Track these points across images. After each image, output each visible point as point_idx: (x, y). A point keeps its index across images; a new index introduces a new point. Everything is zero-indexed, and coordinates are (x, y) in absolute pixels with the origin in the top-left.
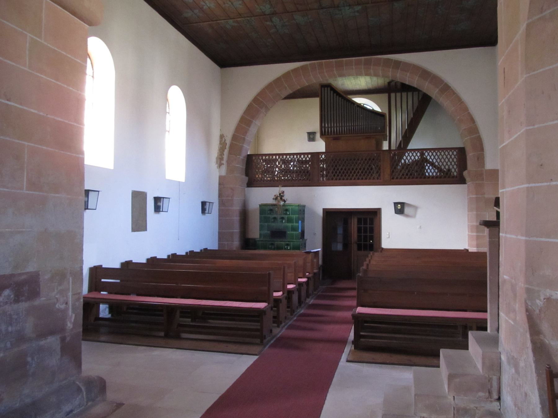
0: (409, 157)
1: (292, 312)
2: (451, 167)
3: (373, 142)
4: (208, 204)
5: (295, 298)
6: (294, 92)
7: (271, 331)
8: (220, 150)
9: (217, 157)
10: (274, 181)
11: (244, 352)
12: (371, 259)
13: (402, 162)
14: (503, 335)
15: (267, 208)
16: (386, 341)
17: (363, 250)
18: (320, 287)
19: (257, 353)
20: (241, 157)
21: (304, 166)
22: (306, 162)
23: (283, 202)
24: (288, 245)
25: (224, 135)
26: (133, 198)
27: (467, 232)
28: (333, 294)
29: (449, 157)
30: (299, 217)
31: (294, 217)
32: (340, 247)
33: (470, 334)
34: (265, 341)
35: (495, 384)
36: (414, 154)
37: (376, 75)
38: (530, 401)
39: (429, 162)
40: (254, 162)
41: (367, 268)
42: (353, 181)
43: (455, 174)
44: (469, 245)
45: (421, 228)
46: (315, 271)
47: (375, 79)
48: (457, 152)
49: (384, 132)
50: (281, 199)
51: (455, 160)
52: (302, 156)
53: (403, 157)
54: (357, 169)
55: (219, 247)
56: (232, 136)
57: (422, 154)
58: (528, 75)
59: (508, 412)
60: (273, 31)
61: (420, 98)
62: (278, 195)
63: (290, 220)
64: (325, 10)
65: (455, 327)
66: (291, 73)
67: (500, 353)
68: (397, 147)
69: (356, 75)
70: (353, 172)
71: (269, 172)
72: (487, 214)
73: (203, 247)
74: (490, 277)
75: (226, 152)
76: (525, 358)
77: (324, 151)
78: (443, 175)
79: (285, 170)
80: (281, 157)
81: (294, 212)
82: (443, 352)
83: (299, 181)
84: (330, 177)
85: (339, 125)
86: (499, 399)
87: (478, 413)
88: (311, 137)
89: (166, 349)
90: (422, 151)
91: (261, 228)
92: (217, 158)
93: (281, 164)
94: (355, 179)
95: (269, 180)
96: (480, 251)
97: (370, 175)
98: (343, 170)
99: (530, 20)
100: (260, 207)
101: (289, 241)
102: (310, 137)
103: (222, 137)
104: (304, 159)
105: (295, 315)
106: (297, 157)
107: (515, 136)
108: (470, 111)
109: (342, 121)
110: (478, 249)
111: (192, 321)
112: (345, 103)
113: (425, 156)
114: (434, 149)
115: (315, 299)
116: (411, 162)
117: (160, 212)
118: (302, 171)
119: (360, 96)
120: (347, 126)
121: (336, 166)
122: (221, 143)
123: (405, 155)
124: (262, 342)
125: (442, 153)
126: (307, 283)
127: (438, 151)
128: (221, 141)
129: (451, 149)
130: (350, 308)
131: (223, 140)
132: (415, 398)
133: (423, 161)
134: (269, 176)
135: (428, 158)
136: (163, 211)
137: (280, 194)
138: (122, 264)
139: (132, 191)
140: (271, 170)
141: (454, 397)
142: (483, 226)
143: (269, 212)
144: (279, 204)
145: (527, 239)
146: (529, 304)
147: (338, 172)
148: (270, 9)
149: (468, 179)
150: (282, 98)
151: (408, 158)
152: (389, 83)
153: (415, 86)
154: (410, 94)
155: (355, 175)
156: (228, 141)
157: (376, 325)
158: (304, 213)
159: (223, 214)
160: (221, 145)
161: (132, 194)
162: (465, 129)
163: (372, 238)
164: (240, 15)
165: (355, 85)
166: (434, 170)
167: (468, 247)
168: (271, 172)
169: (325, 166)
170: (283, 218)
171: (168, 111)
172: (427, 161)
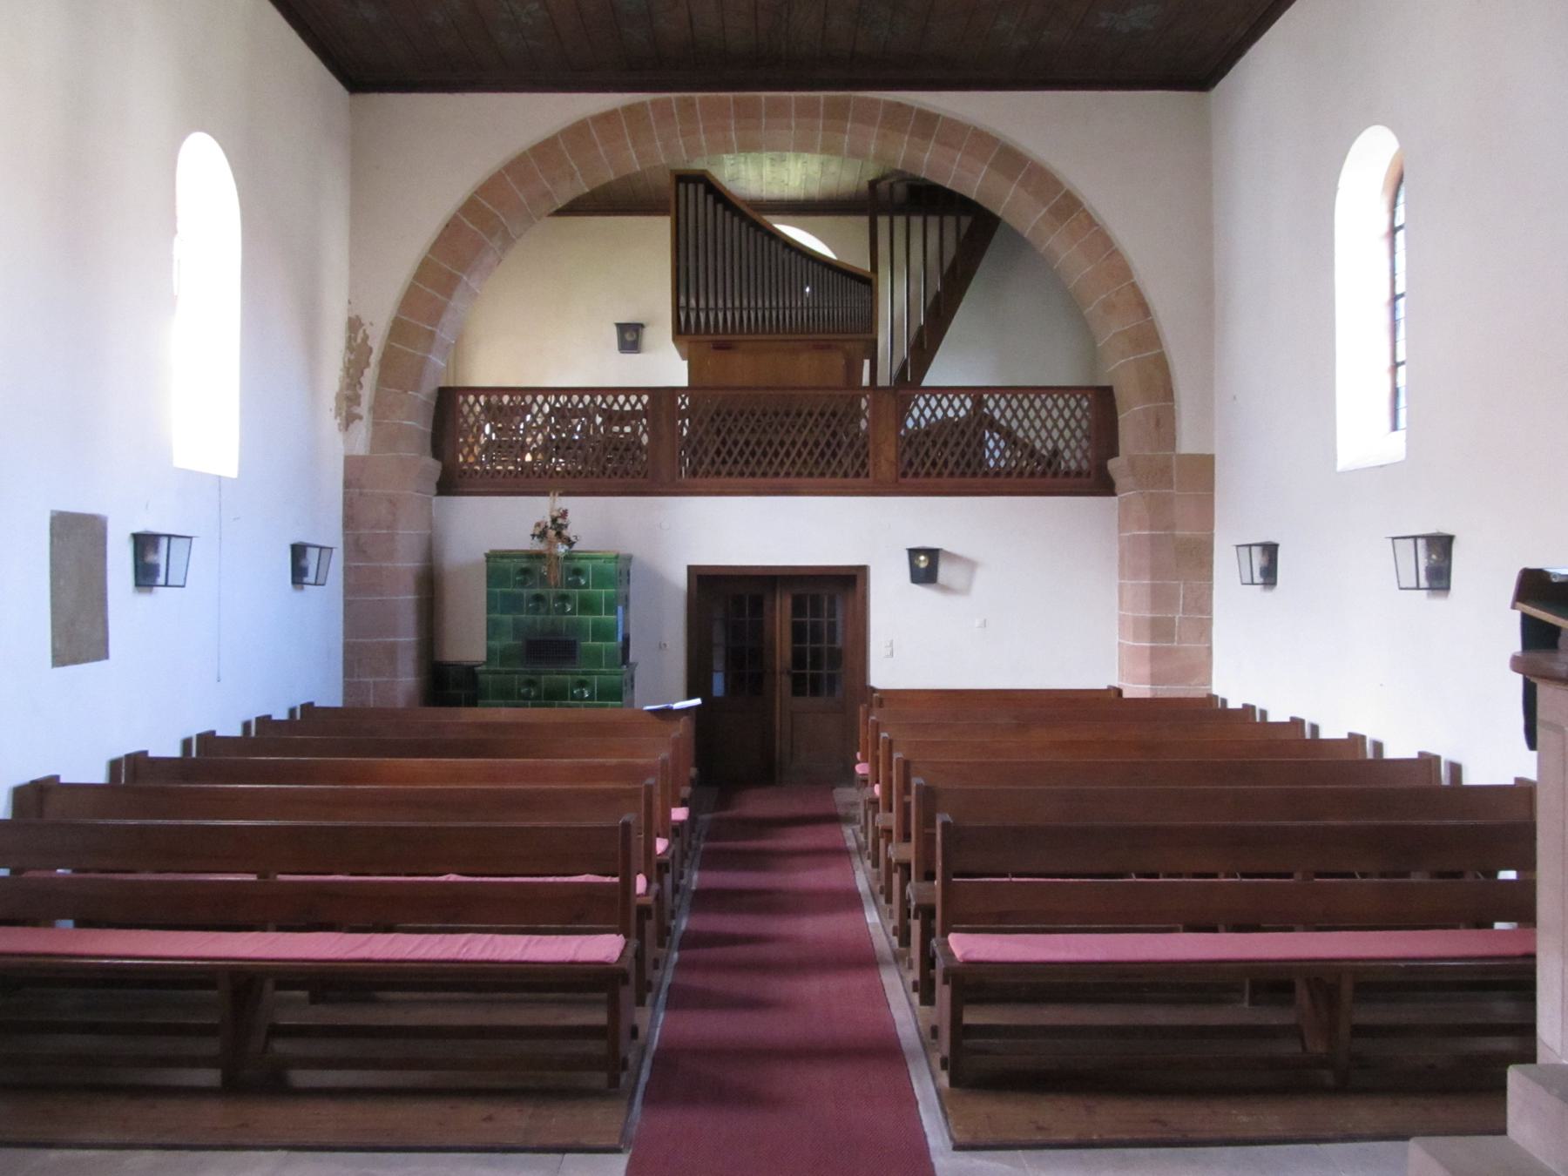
0: (1020, 410)
2: (1061, 444)
3: (839, 361)
8: (347, 370)
11: (568, 1141)
17: (808, 692)
19: (615, 1141)
20: (421, 396)
21: (579, 428)
22: (623, 417)
23: (566, 547)
24: (582, 684)
25: (363, 321)
26: (55, 540)
27: (1117, 637)
42: (780, 480)
50: (559, 534)
51: (1084, 424)
54: (793, 443)
55: (345, 701)
57: (979, 403)
62: (549, 524)
63: (587, 606)
70: (782, 452)
72: (1182, 586)
73: (298, 700)
75: (370, 376)
83: (586, 477)
88: (630, 337)
89: (245, 1154)
91: (493, 629)
94: (788, 474)
100: (487, 561)
101: (585, 673)
102: (626, 341)
103: (354, 325)
104: (627, 408)
108: (1135, 278)
110: (1154, 687)
112: (751, 235)
113: (986, 410)
117: (155, 589)
118: (623, 447)
119: (814, 254)
120: (733, 308)
124: (614, 1081)
128: (350, 340)
129: (957, 390)
131: (360, 335)
135: (997, 414)
136: (170, 583)
137: (554, 520)
139: (52, 511)
143: (518, 578)
144: (553, 551)
149: (1120, 481)
151: (922, 413)
153: (973, 196)
155: (788, 462)
159: (357, 587)
160: (351, 353)
165: (770, 183)
167: (1119, 681)
170: (564, 598)
172: (993, 425)
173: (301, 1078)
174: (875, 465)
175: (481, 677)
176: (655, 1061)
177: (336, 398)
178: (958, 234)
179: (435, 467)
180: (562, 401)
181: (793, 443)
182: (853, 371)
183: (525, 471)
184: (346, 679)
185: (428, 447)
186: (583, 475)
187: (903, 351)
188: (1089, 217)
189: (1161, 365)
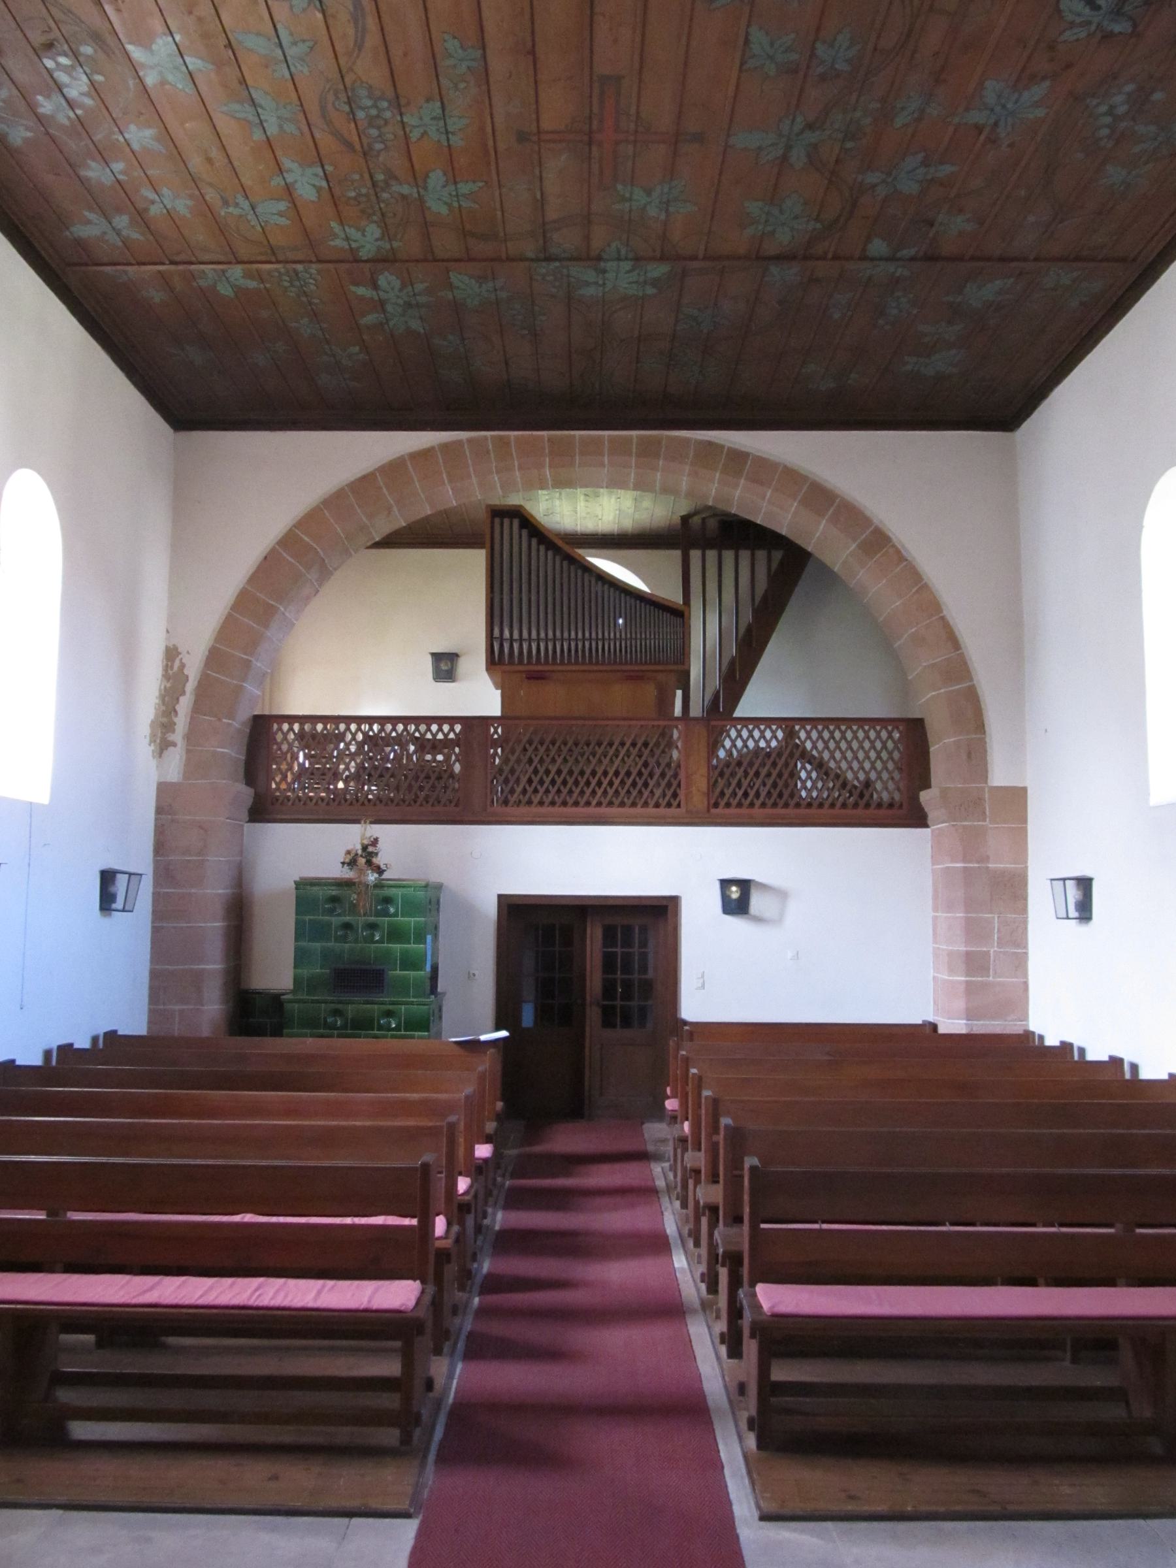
2: (873, 775)
4: (121, 880)
8: (162, 697)
9: (153, 722)
13: (718, 756)
15: (320, 893)
19: (404, 1505)
20: (237, 725)
22: (444, 745)
23: (376, 875)
24: (389, 1014)
27: (932, 971)
30: (425, 921)
31: (411, 922)
42: (591, 810)
44: (936, 1012)
45: (798, 958)
48: (900, 733)
49: (683, 664)
50: (369, 863)
51: (896, 755)
52: (434, 728)
54: (605, 773)
57: (791, 734)
60: (370, 319)
62: (360, 852)
63: (396, 934)
64: (557, 264)
66: (466, 446)
70: (594, 782)
75: (185, 704)
85: (538, 634)
90: (788, 724)
91: (301, 957)
92: (153, 724)
94: (599, 804)
98: (551, 776)
100: (296, 889)
101: (393, 1003)
103: (171, 654)
104: (440, 736)
110: (969, 1022)
113: (797, 741)
122: (166, 676)
124: (406, 1439)
127: (801, 726)
128: (166, 668)
131: (177, 664)
135: (808, 745)
137: (365, 848)
148: (379, 243)
149: (932, 815)
150: (369, 544)
156: (193, 667)
162: (933, 665)
164: (274, 253)
165: (585, 518)
167: (934, 1015)
175: (287, 1006)
179: (246, 793)
182: (665, 703)
187: (715, 682)
188: (898, 552)
189: (972, 698)
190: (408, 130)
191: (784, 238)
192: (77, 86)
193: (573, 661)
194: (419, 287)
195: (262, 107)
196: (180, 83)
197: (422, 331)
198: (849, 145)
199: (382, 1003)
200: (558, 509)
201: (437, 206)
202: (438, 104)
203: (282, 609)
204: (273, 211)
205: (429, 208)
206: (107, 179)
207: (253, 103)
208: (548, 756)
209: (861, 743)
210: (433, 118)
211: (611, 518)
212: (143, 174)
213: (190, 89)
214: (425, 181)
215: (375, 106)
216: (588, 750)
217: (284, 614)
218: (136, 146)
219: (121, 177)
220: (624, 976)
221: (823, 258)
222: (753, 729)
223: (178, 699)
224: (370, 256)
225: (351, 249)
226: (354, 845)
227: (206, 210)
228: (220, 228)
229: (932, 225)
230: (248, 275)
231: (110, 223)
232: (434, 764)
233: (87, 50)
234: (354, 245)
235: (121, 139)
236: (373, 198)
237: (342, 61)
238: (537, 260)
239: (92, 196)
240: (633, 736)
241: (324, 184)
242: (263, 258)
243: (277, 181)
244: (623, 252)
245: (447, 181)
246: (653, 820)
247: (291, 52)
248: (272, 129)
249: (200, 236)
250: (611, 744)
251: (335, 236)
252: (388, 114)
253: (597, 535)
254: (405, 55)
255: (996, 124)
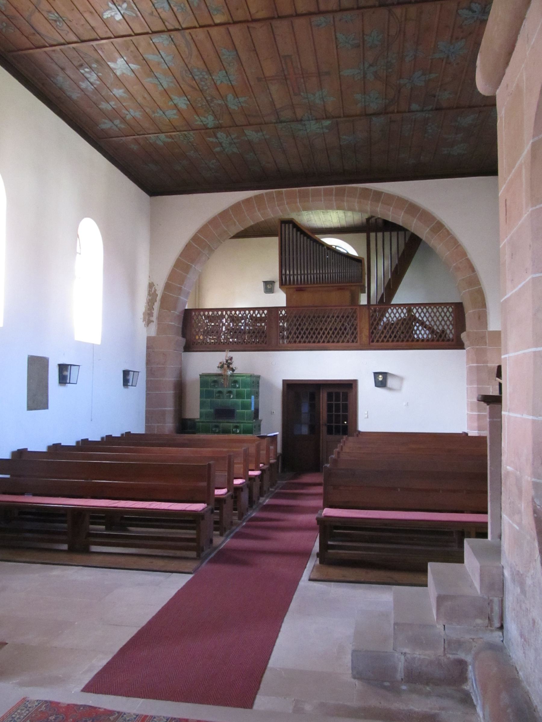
1: (241, 516)
2: (446, 327)
3: (347, 294)
4: (131, 373)
5: (244, 496)
6: (245, 229)
7: (211, 541)
10: (219, 344)
12: (344, 445)
13: (383, 321)
14: (506, 544)
15: (210, 379)
16: (360, 552)
18: (279, 482)
19: (191, 570)
20: (177, 313)
22: (261, 320)
23: (231, 372)
24: (237, 427)
27: (466, 411)
28: (291, 491)
29: (443, 314)
32: (305, 430)
33: (466, 542)
34: (203, 554)
35: (496, 608)
36: (400, 311)
37: (351, 209)
38: (539, 631)
39: (418, 321)
40: (193, 318)
41: (339, 457)
42: (321, 344)
43: (451, 336)
44: (469, 427)
46: (272, 461)
47: (349, 214)
48: (452, 308)
50: (228, 367)
51: (451, 318)
53: (386, 314)
54: (326, 329)
55: (146, 430)
56: (165, 285)
57: (409, 311)
58: (534, 208)
59: (512, 644)
60: (218, 149)
61: (407, 239)
62: (225, 363)
63: (239, 395)
64: (285, 124)
65: (450, 533)
67: (503, 567)
68: (378, 301)
69: (326, 209)
70: (321, 333)
71: (213, 332)
74: (490, 469)
75: (157, 305)
76: (532, 574)
77: (284, 305)
78: (436, 338)
79: (233, 329)
80: (229, 312)
81: (245, 385)
82: (431, 566)
83: (251, 344)
84: (292, 339)
86: (501, 628)
87: (475, 646)
88: (269, 287)
90: (409, 307)
91: (202, 405)
92: (144, 314)
93: (229, 322)
94: (324, 342)
95: (212, 342)
96: (482, 435)
97: (343, 337)
99: (536, 139)
100: (200, 377)
104: (259, 316)
105: (244, 520)
106: (249, 313)
107: (520, 286)
109: (322, 269)
111: (107, 529)
113: (413, 314)
114: (425, 305)
115: (271, 498)
116: (396, 321)
117: (67, 384)
118: (256, 332)
121: (300, 325)
122: (149, 294)
123: (388, 312)
125: (435, 310)
126: (261, 477)
128: (149, 291)
129: (445, 304)
130: (315, 510)
131: (153, 290)
132: (394, 628)
133: (410, 319)
134: (213, 338)
135: (417, 315)
137: (227, 361)
138: (14, 454)
139: (28, 356)
140: (215, 330)
141: (444, 626)
142: (483, 402)
145: (535, 418)
146: (537, 503)
147: (321, 333)
148: (214, 122)
149: (466, 343)
150: (230, 237)
152: (368, 220)
153: (401, 224)
154: (394, 234)
156: (160, 290)
157: (353, 532)
158: (258, 386)
160: (150, 296)
161: (28, 360)
162: (463, 280)
163: (346, 418)
166: (425, 331)
167: (467, 430)
168: (215, 332)
169: (285, 325)
170: (230, 392)
171: (78, 250)
172: (415, 319)
173: (94, 548)
174: (360, 337)
175: (197, 424)
176: (218, 552)
177: (143, 314)
178: (405, 240)
180: (242, 314)
181: (326, 329)
182: (355, 299)
183: (228, 342)
184: (147, 425)
185: (180, 333)
186: (260, 343)
187: (382, 291)
188: (448, 231)
189: (480, 293)
190: (215, 81)
191: (374, 107)
192: (93, 78)
193: (284, 284)
194: (233, 136)
195: (160, 78)
196: (130, 73)
197: (239, 153)
198: (390, 70)
199: (234, 423)
200: (312, 218)
201: (233, 107)
202: (224, 72)
203: (193, 266)
204: (172, 114)
205: (230, 108)
206: (109, 108)
207: (157, 78)
208: (302, 322)
209: (435, 314)
210: (224, 77)
211: (336, 221)
212: (122, 105)
213: (133, 75)
214: (227, 99)
215: (201, 74)
216: (319, 320)
217: (195, 268)
218: (117, 96)
219: (114, 107)
220: (336, 413)
221: (393, 112)
222: (398, 309)
223: (154, 304)
224: (212, 127)
225: (204, 125)
226: (223, 360)
227: (147, 115)
228: (153, 121)
229: (435, 96)
230: (167, 137)
231: (113, 123)
232: (261, 327)
233: (94, 66)
234: (205, 123)
235: (112, 94)
236: (208, 106)
237: (186, 61)
238: (277, 123)
239: (104, 114)
240: (327, 314)
241: (188, 103)
242: (172, 130)
243: (171, 103)
244: (310, 117)
245: (234, 97)
246: (347, 348)
247: (167, 59)
248: (165, 86)
249: (146, 125)
250: (328, 317)
251: (197, 121)
252: (206, 77)
253: (332, 228)
254: (208, 56)
255: (448, 57)
